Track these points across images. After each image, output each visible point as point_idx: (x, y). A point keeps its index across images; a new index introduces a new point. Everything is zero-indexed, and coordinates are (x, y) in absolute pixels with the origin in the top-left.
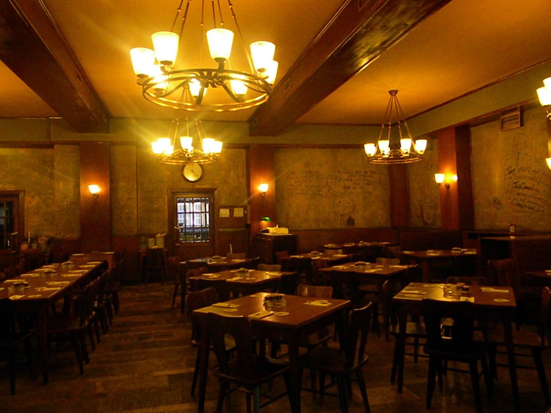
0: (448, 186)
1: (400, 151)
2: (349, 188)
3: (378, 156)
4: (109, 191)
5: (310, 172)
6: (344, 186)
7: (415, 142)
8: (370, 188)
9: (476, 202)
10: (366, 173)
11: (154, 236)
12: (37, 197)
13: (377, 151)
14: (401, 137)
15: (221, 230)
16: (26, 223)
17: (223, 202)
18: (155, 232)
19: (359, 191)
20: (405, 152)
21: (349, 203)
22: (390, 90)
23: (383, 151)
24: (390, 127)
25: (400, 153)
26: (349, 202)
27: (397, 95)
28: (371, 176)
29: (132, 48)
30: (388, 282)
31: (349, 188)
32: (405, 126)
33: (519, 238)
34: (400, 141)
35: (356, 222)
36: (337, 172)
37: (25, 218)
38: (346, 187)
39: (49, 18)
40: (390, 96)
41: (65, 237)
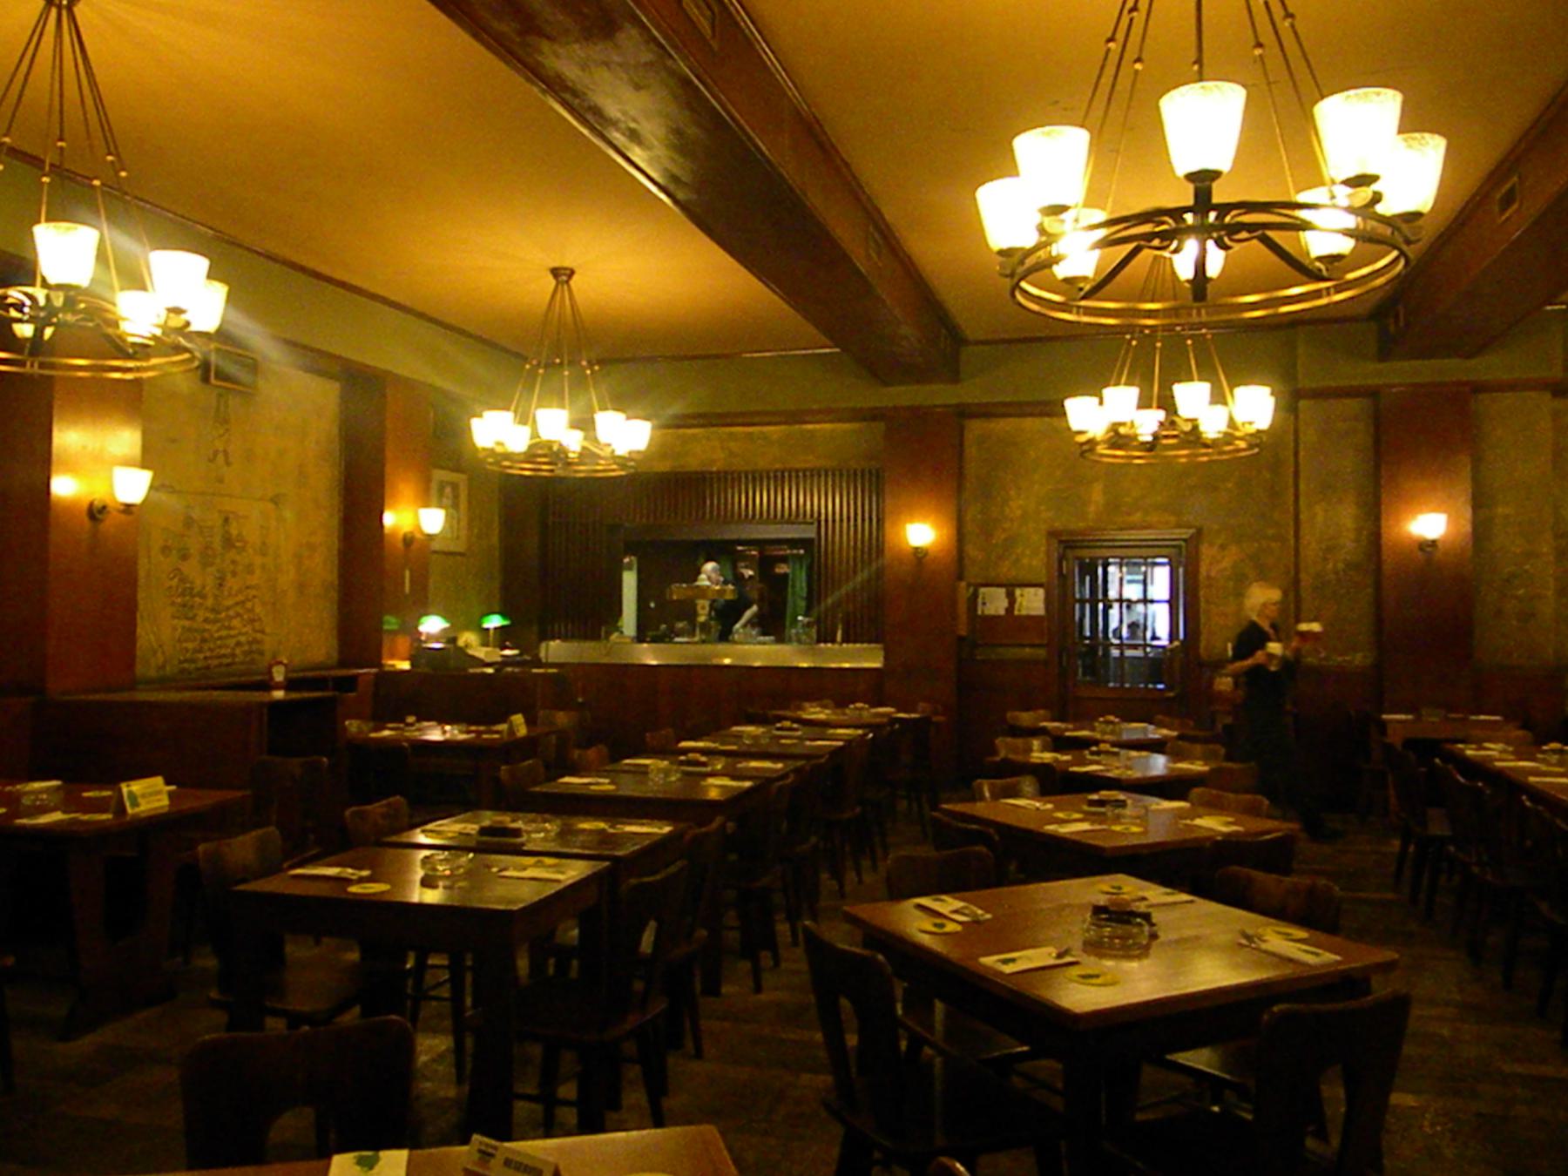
4: (1468, 528)
24: (1159, 345)
27: (572, 283)
33: (295, 695)
37: (1203, 605)
39: (799, 107)
40: (553, 282)
41: (1331, 663)
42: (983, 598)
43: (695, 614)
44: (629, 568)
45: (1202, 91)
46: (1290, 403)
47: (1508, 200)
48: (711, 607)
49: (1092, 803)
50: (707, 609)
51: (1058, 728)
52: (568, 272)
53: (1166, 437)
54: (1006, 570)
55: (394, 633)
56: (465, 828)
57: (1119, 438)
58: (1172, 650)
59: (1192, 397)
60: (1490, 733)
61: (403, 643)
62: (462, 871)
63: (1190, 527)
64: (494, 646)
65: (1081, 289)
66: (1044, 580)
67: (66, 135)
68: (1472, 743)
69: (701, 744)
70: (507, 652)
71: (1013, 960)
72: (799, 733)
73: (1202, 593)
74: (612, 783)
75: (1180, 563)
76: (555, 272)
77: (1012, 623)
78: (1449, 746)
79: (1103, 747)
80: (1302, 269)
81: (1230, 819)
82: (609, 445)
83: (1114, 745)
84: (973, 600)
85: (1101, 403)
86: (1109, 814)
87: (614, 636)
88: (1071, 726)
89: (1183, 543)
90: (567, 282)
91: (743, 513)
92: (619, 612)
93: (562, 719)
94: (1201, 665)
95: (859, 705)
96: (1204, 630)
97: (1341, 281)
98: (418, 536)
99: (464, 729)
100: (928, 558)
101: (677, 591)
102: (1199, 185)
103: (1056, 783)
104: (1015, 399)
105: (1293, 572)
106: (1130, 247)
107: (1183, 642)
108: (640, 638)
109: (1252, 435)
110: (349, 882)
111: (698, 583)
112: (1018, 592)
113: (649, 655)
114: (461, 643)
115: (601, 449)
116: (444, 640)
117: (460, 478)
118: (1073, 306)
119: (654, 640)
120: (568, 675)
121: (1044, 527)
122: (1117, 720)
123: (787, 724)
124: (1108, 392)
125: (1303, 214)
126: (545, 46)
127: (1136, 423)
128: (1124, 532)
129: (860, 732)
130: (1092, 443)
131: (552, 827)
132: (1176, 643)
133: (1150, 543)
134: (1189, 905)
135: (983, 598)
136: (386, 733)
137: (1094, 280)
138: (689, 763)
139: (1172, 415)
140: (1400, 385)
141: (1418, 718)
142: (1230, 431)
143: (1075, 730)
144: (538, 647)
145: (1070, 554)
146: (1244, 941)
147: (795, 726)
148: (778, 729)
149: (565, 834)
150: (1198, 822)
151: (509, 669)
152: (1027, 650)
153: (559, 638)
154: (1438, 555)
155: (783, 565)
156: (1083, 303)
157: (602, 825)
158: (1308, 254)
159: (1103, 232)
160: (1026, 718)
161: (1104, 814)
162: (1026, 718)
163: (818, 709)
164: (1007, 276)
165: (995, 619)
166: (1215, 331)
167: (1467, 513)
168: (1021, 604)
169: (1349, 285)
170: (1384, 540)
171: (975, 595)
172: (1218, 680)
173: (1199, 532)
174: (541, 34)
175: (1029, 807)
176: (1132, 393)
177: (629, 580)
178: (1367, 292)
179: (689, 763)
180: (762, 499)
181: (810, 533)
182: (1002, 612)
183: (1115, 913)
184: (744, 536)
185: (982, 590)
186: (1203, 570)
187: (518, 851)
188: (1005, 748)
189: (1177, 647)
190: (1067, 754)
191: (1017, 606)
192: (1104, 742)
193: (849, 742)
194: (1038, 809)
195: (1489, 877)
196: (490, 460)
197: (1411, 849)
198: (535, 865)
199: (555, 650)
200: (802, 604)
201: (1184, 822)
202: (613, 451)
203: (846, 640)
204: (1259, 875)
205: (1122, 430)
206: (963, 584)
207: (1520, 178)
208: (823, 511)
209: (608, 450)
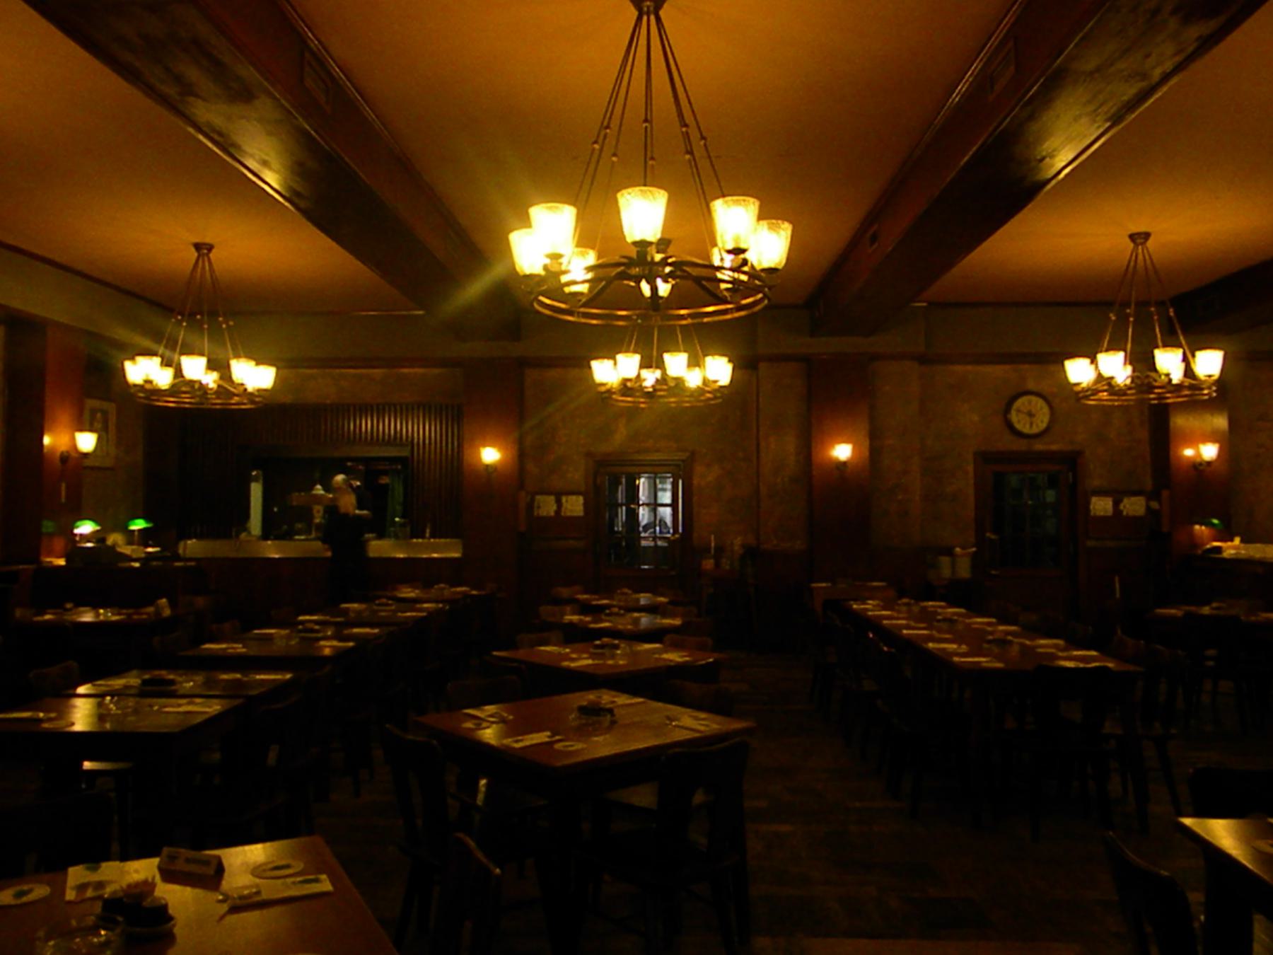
3: (1099, 386)
4: (867, 453)
11: (949, 552)
15: (1090, 543)
17: (1096, 483)
22: (1130, 233)
27: (211, 255)
40: (1132, 245)
43: (312, 517)
44: (256, 479)
45: (640, 192)
46: (743, 365)
48: (325, 512)
49: (597, 647)
50: (322, 512)
51: (587, 599)
52: (208, 247)
53: (661, 390)
55: (51, 535)
56: (127, 682)
57: (627, 388)
58: (674, 541)
59: (676, 363)
61: (59, 544)
62: (129, 710)
64: (139, 544)
65: (580, 301)
66: (583, 489)
69: (315, 618)
70: (150, 550)
71: (521, 741)
72: (393, 608)
74: (244, 647)
76: (198, 246)
77: (560, 522)
79: (615, 610)
81: (684, 654)
82: (242, 384)
83: (620, 608)
84: (530, 506)
85: (615, 364)
87: (243, 535)
88: (597, 597)
89: (680, 463)
90: (207, 255)
91: (358, 436)
92: (246, 515)
93: (200, 602)
95: (442, 585)
98: (74, 454)
99: (116, 612)
101: (297, 498)
103: (576, 636)
107: (682, 534)
108: (265, 536)
110: (40, 721)
111: (314, 492)
112: (564, 499)
113: (272, 551)
114: (110, 542)
115: (235, 388)
116: (94, 540)
117: (111, 407)
119: (277, 538)
120: (202, 567)
122: (630, 592)
123: (384, 600)
124: (620, 357)
126: (200, 102)
129: (441, 605)
130: (610, 392)
131: (200, 678)
132: (677, 536)
136: (48, 617)
137: (587, 295)
138: (306, 630)
142: (704, 387)
143: (598, 600)
144: (176, 544)
147: (390, 602)
148: (379, 605)
149: (209, 684)
150: (665, 656)
151: (154, 563)
152: (571, 542)
153: (195, 537)
155: (384, 477)
156: (582, 310)
157: (238, 676)
160: (565, 592)
162: (565, 592)
163: (409, 590)
165: (547, 519)
167: (867, 443)
171: (533, 500)
172: (704, 562)
173: (693, 453)
174: (197, 96)
176: (636, 358)
177: (256, 490)
179: (306, 630)
180: (367, 424)
181: (405, 453)
182: (552, 514)
184: (353, 455)
185: (538, 497)
187: (174, 695)
188: (546, 611)
189: (678, 538)
191: (563, 509)
192: (614, 606)
193: (431, 613)
196: (141, 395)
198: (189, 704)
199: (192, 547)
200: (399, 508)
202: (246, 390)
203: (433, 536)
205: (629, 384)
206: (523, 494)
208: (416, 435)
209: (241, 389)
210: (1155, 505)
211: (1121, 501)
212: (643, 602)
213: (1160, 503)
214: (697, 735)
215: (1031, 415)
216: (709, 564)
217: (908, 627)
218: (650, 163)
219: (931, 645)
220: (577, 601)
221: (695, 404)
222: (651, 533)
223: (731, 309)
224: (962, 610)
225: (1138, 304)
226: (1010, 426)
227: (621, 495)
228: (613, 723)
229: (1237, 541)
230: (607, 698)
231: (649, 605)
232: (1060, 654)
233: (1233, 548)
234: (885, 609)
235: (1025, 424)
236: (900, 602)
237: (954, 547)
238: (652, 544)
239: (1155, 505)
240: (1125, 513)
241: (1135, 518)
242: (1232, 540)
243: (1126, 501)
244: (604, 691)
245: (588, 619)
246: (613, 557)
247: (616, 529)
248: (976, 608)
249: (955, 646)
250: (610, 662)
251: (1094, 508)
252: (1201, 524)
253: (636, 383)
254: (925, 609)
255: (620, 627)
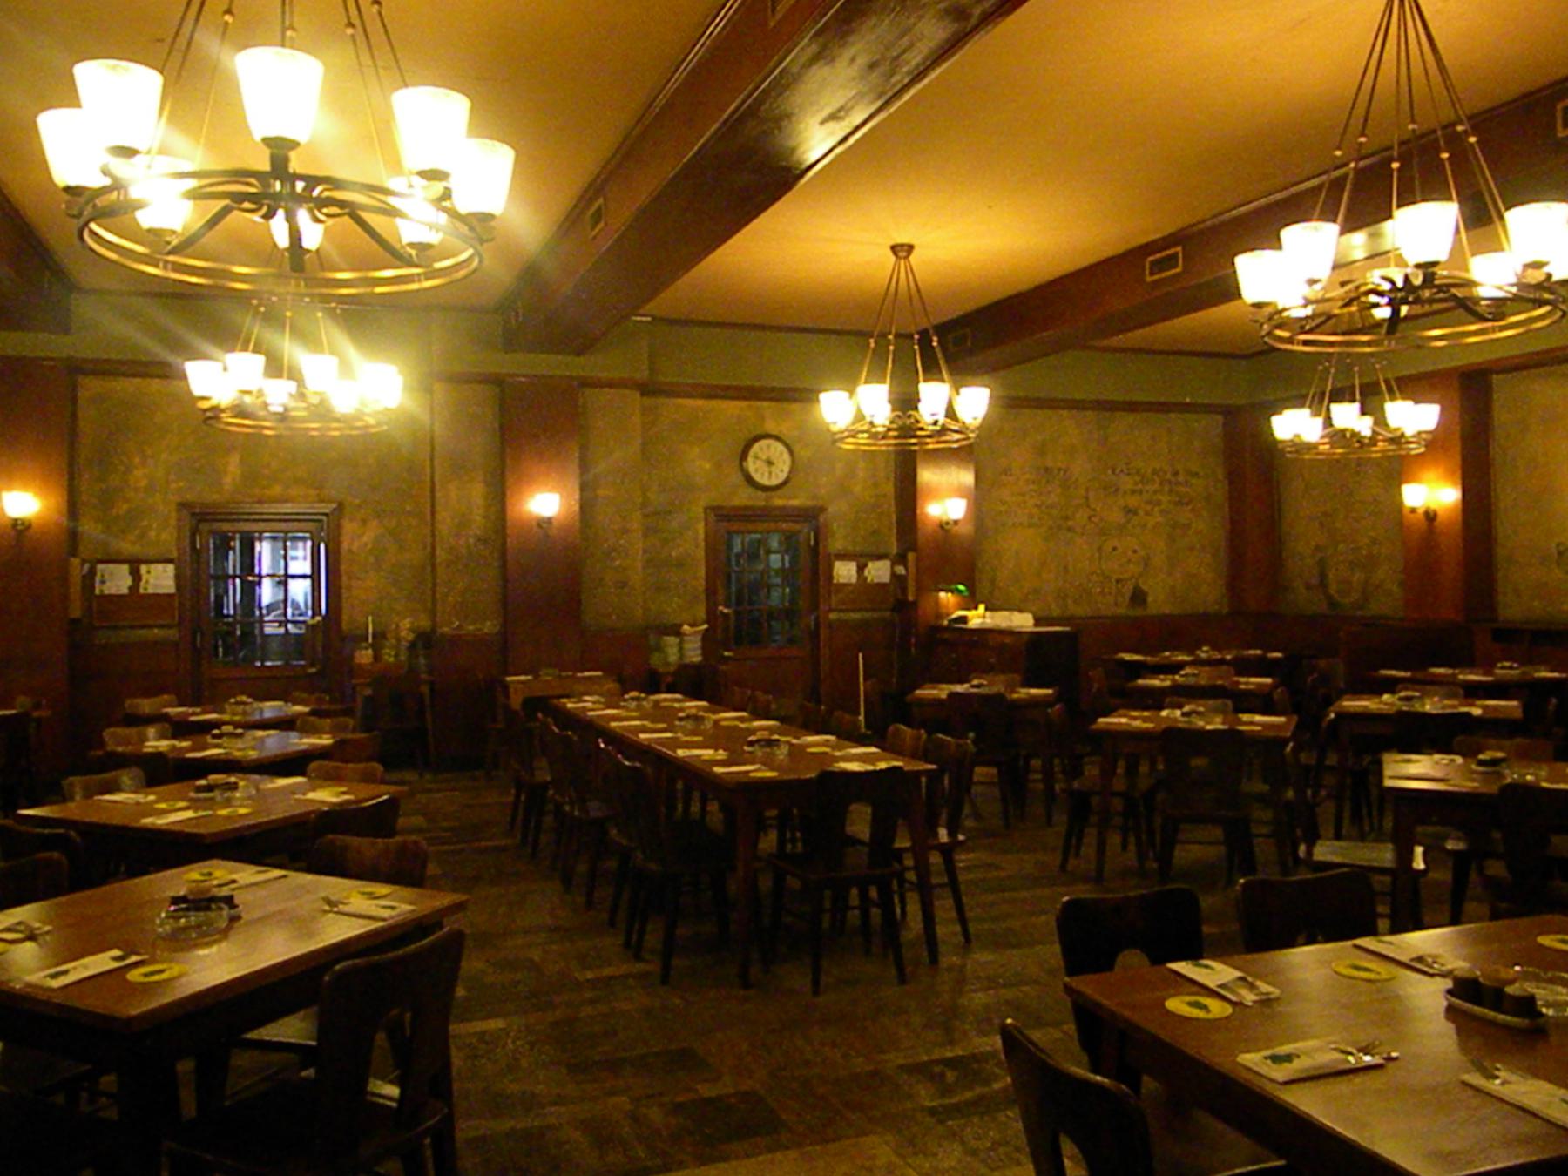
0: (1430, 516)
1: (919, 418)
2: (1136, 513)
3: (858, 427)
4: (576, 508)
5: (1047, 470)
6: (1125, 507)
7: (958, 393)
8: (1184, 515)
9: (1501, 553)
10: (1176, 474)
11: (676, 631)
12: (375, 522)
13: (955, 414)
14: (921, 378)
15: (833, 616)
16: (344, 592)
18: (678, 621)
19: (1160, 519)
20: (930, 420)
21: (1135, 551)
22: (892, 243)
23: (873, 416)
25: (918, 422)
26: (1136, 547)
27: (912, 258)
28: (1186, 483)
29: (397, 89)
30: (1294, 747)
31: (1136, 513)
32: (933, 347)
34: (917, 387)
35: (1150, 599)
36: (1110, 472)
38: (1130, 511)
40: (893, 258)
41: (463, 632)
42: (102, 576)
47: (598, 216)
49: (200, 789)
54: (128, 547)
60: (589, 687)
63: (330, 501)
65: (168, 243)
66: (175, 555)
67: (1417, 118)
68: (573, 697)
71: (65, 972)
73: (343, 567)
75: (322, 539)
78: (555, 701)
80: (395, 255)
81: (344, 789)
83: (237, 725)
86: (219, 798)
94: (343, 639)
96: (345, 605)
97: (430, 269)
100: (31, 531)
102: (275, 151)
103: (160, 772)
104: (735, 383)
105: (429, 549)
106: (220, 204)
109: (379, 412)
112: (143, 568)
118: (159, 260)
121: (175, 499)
122: (250, 700)
125: (391, 200)
127: (266, 391)
128: (274, 505)
130: (216, 409)
132: (318, 618)
133: (287, 517)
134: (282, 880)
135: (102, 576)
137: (183, 234)
139: (912, 409)
140: (524, 376)
141: (537, 676)
145: (204, 527)
146: (327, 908)
150: (311, 795)
152: (156, 631)
154: (553, 532)
156: (171, 258)
158: (400, 241)
159: (192, 183)
160: (146, 705)
161: (212, 799)
162: (146, 705)
164: (74, 216)
166: (346, 307)
168: (147, 582)
169: (436, 274)
170: (508, 518)
171: (92, 572)
173: (341, 506)
175: (129, 801)
178: (452, 282)
182: (125, 591)
183: (193, 901)
185: (100, 567)
186: (345, 546)
188: (115, 739)
189: (319, 622)
190: (186, 740)
191: (142, 584)
194: (138, 804)
195: (576, 813)
197: (523, 798)
201: (297, 796)
204: (354, 841)
206: (75, 561)
207: (605, 199)
210: (901, 570)
211: (866, 565)
212: (268, 714)
213: (906, 569)
214: (381, 924)
215: (770, 463)
216: (364, 656)
217: (644, 730)
218: (289, 33)
219: (681, 753)
220: (165, 718)
221: (348, 432)
222: (279, 615)
223: (419, 275)
224: (704, 703)
225: (897, 336)
226: (749, 480)
227: (233, 561)
228: (234, 919)
229: (982, 608)
230: (222, 874)
231: (276, 718)
232: (838, 754)
233: (977, 618)
234: (609, 707)
235: (763, 474)
236: (627, 696)
237: (681, 625)
238: (282, 630)
239: (901, 570)
240: (869, 580)
241: (882, 586)
242: (976, 608)
243: (871, 565)
244: (215, 862)
245: (185, 744)
246: (221, 650)
247: (225, 611)
248: (719, 701)
249: (711, 752)
250: (224, 812)
251: (838, 574)
252: (947, 591)
253: (258, 398)
254: (657, 703)
255: (238, 754)
